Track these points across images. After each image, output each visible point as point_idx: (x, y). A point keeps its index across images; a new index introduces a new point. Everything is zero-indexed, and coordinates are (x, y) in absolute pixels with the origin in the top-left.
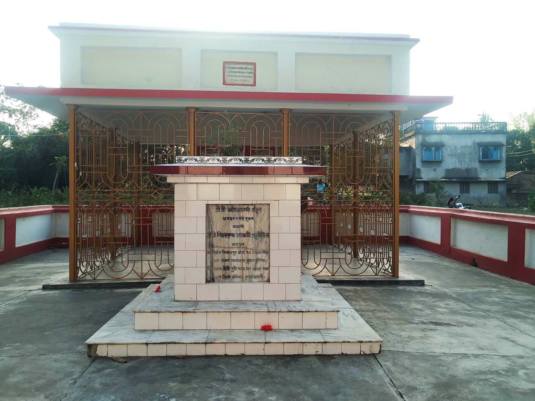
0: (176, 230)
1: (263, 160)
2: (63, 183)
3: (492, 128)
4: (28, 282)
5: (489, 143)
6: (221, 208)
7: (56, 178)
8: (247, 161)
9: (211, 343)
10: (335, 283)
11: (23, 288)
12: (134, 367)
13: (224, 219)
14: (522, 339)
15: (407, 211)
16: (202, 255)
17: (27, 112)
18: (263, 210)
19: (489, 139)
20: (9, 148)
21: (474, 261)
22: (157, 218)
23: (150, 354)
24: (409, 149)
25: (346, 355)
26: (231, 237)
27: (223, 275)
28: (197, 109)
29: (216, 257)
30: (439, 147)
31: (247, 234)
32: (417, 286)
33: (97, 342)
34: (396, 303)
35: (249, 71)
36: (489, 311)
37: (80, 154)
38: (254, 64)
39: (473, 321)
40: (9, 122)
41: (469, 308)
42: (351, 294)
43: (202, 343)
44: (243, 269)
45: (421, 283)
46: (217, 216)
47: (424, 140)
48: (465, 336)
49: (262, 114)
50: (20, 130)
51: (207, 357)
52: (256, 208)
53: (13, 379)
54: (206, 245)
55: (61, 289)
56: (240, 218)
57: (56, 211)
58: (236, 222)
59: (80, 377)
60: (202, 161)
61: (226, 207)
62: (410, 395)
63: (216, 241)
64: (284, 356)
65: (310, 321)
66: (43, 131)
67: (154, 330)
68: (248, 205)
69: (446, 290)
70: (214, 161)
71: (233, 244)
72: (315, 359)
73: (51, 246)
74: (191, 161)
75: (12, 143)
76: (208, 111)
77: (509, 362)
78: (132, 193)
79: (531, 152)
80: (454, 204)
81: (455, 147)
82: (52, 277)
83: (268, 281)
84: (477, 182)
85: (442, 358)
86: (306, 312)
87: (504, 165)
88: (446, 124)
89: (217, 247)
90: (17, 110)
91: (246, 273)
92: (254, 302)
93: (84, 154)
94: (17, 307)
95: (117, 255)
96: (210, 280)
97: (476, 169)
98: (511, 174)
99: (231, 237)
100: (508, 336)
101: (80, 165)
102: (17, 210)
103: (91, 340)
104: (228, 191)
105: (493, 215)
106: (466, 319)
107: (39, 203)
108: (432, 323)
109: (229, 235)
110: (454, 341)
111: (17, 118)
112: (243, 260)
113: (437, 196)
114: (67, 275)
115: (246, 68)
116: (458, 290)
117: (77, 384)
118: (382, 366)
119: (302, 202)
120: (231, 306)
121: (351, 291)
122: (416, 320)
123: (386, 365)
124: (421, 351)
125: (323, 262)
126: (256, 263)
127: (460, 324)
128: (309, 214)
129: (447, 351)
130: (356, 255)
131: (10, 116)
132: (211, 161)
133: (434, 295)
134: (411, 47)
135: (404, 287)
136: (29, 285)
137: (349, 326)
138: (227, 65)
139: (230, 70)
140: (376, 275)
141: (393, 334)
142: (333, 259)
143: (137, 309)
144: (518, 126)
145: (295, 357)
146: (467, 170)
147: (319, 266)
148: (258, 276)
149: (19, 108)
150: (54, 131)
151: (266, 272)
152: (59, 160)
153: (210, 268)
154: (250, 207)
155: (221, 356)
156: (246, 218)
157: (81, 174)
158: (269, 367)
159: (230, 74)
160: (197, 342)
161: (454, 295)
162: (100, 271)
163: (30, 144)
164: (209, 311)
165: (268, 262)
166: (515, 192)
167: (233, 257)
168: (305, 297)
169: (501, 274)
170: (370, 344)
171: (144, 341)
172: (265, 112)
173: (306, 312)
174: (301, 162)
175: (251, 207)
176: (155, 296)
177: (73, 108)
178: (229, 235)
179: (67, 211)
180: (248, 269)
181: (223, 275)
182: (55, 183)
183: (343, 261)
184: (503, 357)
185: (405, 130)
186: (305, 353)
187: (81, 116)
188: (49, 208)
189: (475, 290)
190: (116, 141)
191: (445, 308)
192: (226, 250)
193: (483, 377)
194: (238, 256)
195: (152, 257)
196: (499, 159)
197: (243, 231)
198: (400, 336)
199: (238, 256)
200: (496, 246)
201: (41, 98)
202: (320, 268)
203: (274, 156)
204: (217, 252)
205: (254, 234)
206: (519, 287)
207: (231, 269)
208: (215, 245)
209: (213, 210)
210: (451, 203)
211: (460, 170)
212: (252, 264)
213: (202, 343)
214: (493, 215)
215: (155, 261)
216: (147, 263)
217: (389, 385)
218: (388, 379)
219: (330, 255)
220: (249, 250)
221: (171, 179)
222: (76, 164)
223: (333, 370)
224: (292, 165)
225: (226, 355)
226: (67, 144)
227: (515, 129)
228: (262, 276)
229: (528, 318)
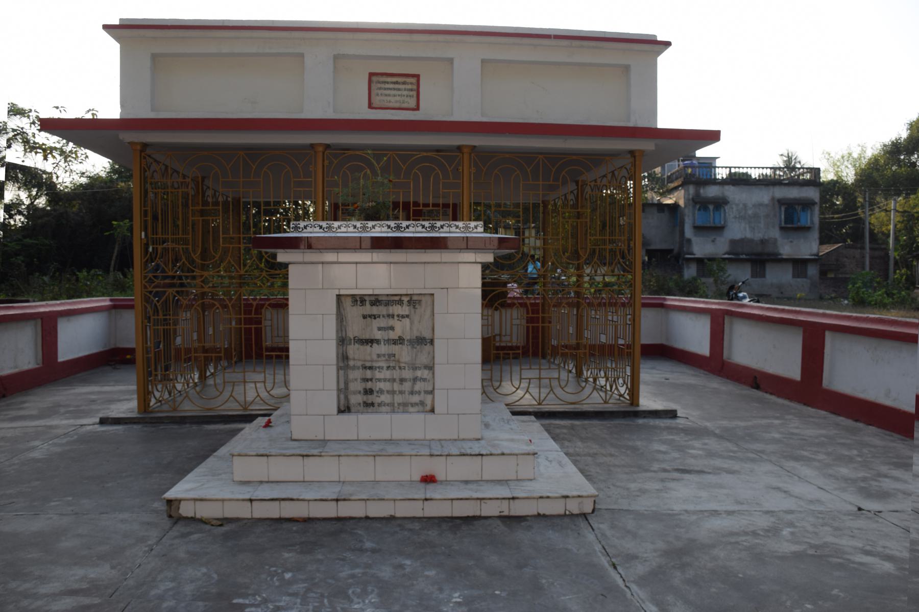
0: (292, 334)
1: (423, 227)
2: (125, 263)
3: (798, 176)
4: (78, 413)
5: (795, 199)
6: (359, 300)
7: (115, 254)
8: (398, 228)
9: (344, 500)
10: (540, 415)
11: (72, 422)
12: (232, 530)
13: (364, 317)
14: (799, 488)
15: (662, 306)
16: (331, 373)
17: (71, 152)
18: (423, 303)
19: (794, 193)
20: (44, 209)
21: (756, 380)
22: (268, 314)
23: (257, 515)
24: (675, 207)
25: (544, 516)
27: (364, 402)
28: (328, 146)
30: (720, 203)
31: (400, 341)
32: (666, 418)
33: (179, 496)
34: (630, 443)
35: (410, 87)
36: (762, 452)
37: (149, 218)
38: (417, 77)
39: (736, 466)
40: (43, 169)
41: (736, 449)
42: (565, 431)
43: (332, 500)
44: (392, 392)
45: (672, 414)
46: (354, 313)
47: (697, 194)
48: (721, 487)
49: (507, 156)
50: (60, 180)
51: (339, 519)
52: (413, 301)
53: (66, 544)
54: (337, 357)
55: (126, 423)
56: (389, 316)
57: (116, 307)
58: (382, 322)
59: (157, 543)
61: (367, 298)
62: (627, 565)
63: (354, 350)
64: (452, 518)
65: (493, 468)
66: (95, 180)
67: (261, 482)
68: (401, 295)
69: (708, 424)
70: (346, 229)
71: (379, 356)
72: (499, 522)
73: (110, 359)
74: (312, 230)
75: (48, 200)
77: (772, 519)
78: (231, 278)
79: (857, 214)
80: (736, 294)
81: (745, 205)
82: (113, 407)
83: (432, 411)
84: (777, 259)
85: (682, 517)
86: (487, 455)
87: (815, 235)
88: (730, 168)
89: (354, 359)
90: (56, 149)
91: (398, 399)
92: (410, 442)
93: (155, 218)
95: (208, 374)
96: (345, 409)
97: (776, 240)
98: (827, 249)
99: (375, 345)
100: (780, 485)
101: (150, 236)
102: (58, 305)
103: (171, 494)
104: (376, 274)
105: (783, 311)
106: (726, 464)
107: (89, 295)
108: (677, 470)
109: (371, 342)
110: (704, 494)
111: (55, 161)
112: (394, 380)
113: (716, 281)
114: (134, 404)
115: (404, 83)
116: (725, 423)
117: (153, 552)
118: (593, 530)
119: (483, 291)
120: (376, 448)
121: (564, 427)
122: (656, 466)
123: (599, 529)
124: (654, 509)
125: (524, 384)
127: (717, 471)
128: (503, 311)
129: (691, 507)
130: (579, 374)
131: (45, 158)
132: (343, 229)
133: (687, 431)
134: (660, 53)
135: (645, 421)
136: (80, 418)
137: (552, 473)
138: (374, 79)
139: (379, 85)
140: (606, 402)
141: (618, 487)
142: (540, 379)
143: (236, 452)
144: (840, 174)
145: (469, 520)
146: (763, 242)
147: (521, 388)
148: (416, 404)
149: (58, 146)
150: (111, 181)
151: (429, 397)
152: (119, 226)
153: (343, 390)
154: (404, 298)
155: (361, 518)
156: (398, 316)
157: (151, 249)
158: (430, 533)
159: (380, 92)
160: (324, 498)
161: (717, 431)
162: (182, 398)
163: (74, 202)
164: (343, 453)
165: (431, 382)
166: (832, 276)
167: (378, 375)
168: (488, 434)
169: (790, 399)
170: (580, 500)
171: (248, 497)
172: (438, 150)
173: (487, 455)
174: (482, 230)
175: (405, 299)
176: (264, 433)
177: (139, 147)
178: (371, 342)
179: (132, 307)
180: (401, 392)
181: (364, 402)
182: (113, 263)
183: (555, 383)
184: (767, 512)
185: (669, 177)
186: (484, 513)
187: (151, 160)
188: (104, 301)
189: (750, 423)
190: (203, 196)
191: (699, 449)
192: (368, 364)
193: (733, 540)
194: (387, 374)
195: (260, 377)
196: (809, 224)
197: (393, 335)
198: (628, 489)
199: (387, 374)
200: (782, 357)
201: (81, 131)
202: (520, 393)
203: (408, 219)
204: (354, 368)
205: (410, 341)
206: (813, 417)
207: (375, 393)
209: (348, 303)
210: (731, 293)
211: (751, 241)
212: (407, 386)
213: (332, 500)
214: (783, 311)
215: (264, 382)
216: (253, 386)
217: (600, 554)
218: (600, 546)
219: (533, 374)
220: (402, 365)
221: (282, 256)
222: (143, 233)
223: (521, 535)
224: (468, 235)
225: (367, 518)
226: (130, 200)
227: (835, 179)
228: (422, 403)
229: (814, 460)
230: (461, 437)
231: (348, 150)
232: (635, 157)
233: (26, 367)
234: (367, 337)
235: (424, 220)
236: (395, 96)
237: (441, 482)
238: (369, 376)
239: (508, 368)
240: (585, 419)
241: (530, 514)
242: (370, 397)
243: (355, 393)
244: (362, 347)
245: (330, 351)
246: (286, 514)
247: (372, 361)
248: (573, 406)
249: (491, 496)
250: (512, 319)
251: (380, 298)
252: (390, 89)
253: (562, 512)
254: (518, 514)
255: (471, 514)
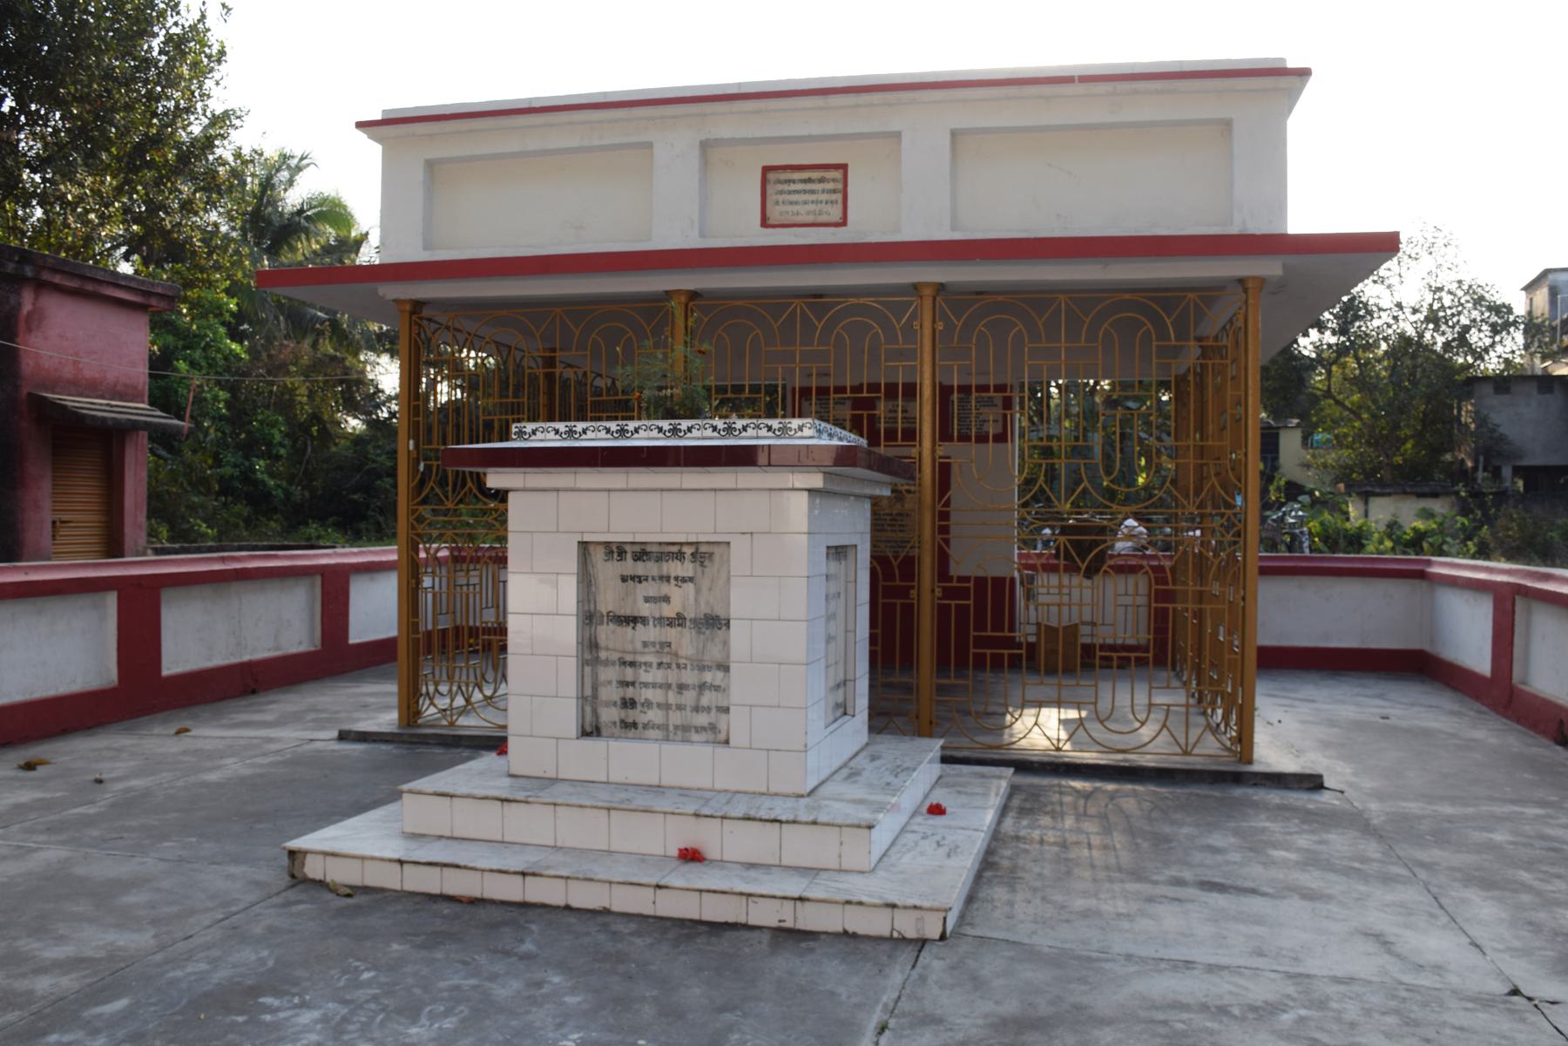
6: (616, 551)
9: (534, 874)
13: (624, 579)
15: (1421, 575)
16: (570, 667)
18: (717, 558)
25: (855, 936)
26: (639, 626)
27: (622, 721)
29: (609, 674)
31: (679, 621)
35: (831, 186)
38: (843, 167)
43: (516, 873)
44: (666, 707)
45: (1313, 783)
46: (607, 572)
49: (1127, 296)
51: (525, 905)
52: (701, 554)
55: (375, 741)
56: (661, 578)
57: (457, 559)
58: (651, 589)
60: (571, 432)
61: (628, 548)
63: (607, 634)
71: (645, 644)
76: (838, 296)
83: (727, 742)
86: (787, 822)
89: (607, 649)
91: (675, 718)
92: (684, 791)
94: (258, 771)
96: (591, 731)
99: (639, 626)
102: (355, 554)
103: (295, 844)
109: (633, 620)
112: (669, 686)
114: (394, 715)
115: (821, 180)
125: (1158, 716)
126: (700, 694)
138: (771, 176)
139: (780, 187)
148: (704, 729)
153: (589, 699)
156: (676, 578)
157: (421, 467)
159: (780, 198)
164: (559, 801)
167: (645, 676)
170: (918, 913)
173: (787, 822)
175: (688, 550)
177: (408, 307)
178: (633, 620)
180: (680, 707)
181: (622, 721)
189: (1470, 810)
192: (629, 658)
197: (669, 611)
203: (584, 419)
204: (607, 663)
205: (695, 621)
208: (602, 643)
209: (598, 555)
212: (689, 697)
220: (682, 661)
221: (496, 479)
225: (568, 908)
228: (713, 728)
230: (772, 790)
231: (821, 296)
232: (1246, 291)
233: (294, 650)
234: (628, 613)
235: (609, 419)
236: (805, 203)
237: (712, 861)
238: (629, 678)
239: (1109, 685)
240: (1132, 781)
241: (830, 929)
242: (631, 712)
243: (609, 704)
244: (619, 629)
245: (567, 631)
246: (451, 890)
247: (635, 653)
248: (1120, 756)
249: (764, 892)
250: (1116, 595)
251: (649, 549)
252: (798, 192)
253: (886, 933)
254: (809, 928)
255: (731, 920)
